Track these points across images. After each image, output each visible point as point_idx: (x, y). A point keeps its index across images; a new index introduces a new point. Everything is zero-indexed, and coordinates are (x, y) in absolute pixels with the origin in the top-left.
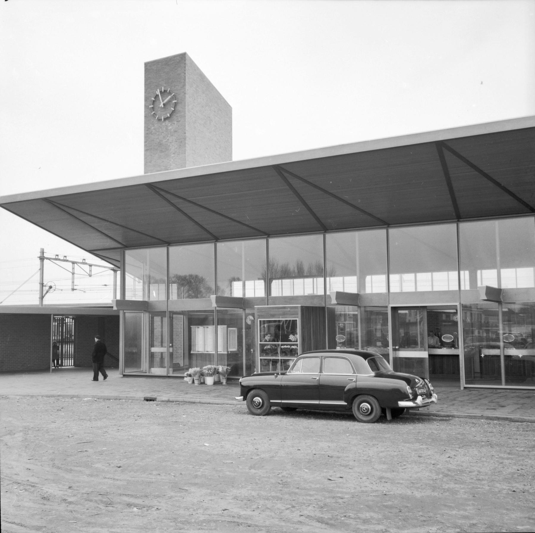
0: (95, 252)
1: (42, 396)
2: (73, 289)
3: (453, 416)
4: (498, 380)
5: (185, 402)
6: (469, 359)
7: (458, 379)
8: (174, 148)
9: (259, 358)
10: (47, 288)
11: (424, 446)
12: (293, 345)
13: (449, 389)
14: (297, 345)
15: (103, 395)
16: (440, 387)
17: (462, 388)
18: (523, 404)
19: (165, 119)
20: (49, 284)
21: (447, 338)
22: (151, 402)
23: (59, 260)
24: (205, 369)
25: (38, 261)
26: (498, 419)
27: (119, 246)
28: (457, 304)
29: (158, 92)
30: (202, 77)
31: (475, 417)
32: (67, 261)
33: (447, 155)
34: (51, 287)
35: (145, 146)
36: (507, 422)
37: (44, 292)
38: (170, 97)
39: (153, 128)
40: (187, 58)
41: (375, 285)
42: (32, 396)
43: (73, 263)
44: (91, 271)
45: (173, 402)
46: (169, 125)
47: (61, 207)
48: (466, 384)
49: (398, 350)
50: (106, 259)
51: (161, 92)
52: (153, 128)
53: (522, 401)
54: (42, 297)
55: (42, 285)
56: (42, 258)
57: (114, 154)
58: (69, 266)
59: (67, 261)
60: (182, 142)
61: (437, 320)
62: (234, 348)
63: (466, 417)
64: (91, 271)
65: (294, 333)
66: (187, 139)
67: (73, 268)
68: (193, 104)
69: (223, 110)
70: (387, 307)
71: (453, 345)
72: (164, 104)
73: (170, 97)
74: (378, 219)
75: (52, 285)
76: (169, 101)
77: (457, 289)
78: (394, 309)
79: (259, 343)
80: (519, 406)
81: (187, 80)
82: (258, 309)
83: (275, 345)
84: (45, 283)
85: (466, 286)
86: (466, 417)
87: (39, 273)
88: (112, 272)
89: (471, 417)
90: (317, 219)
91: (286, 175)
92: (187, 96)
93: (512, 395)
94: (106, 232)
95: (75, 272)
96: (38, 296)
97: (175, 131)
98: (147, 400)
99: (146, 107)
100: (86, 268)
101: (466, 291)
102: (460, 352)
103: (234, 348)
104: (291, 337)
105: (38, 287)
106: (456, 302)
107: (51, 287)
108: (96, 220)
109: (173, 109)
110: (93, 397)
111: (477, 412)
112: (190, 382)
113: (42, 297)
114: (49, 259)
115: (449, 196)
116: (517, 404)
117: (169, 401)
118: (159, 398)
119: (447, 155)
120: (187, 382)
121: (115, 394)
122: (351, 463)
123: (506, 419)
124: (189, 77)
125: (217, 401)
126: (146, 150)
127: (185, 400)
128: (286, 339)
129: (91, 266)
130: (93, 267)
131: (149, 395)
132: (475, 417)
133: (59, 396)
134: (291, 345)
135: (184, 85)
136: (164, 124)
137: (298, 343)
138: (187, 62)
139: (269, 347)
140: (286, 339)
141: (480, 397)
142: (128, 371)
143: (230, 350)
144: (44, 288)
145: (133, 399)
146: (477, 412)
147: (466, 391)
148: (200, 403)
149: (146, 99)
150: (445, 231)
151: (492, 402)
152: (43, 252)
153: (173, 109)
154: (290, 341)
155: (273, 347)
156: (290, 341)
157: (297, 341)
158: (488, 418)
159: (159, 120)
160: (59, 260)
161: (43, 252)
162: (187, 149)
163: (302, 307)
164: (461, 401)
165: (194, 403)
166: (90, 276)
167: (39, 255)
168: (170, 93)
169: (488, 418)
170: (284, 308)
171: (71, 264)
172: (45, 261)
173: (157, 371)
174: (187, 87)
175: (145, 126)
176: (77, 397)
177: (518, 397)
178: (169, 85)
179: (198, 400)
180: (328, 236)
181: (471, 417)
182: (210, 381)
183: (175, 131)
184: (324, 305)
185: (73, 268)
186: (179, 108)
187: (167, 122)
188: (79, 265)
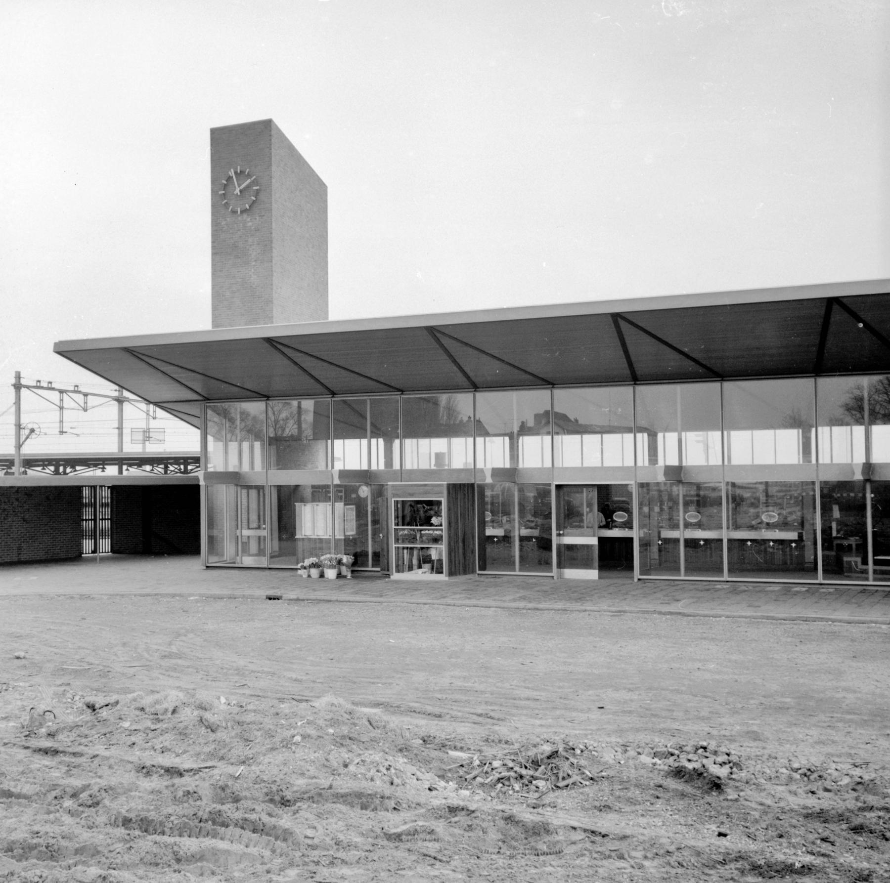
0: (164, 405)
1: (135, 595)
2: (62, 432)
3: (625, 612)
4: (677, 570)
5: (320, 601)
6: (645, 545)
7: (631, 568)
8: (255, 253)
9: (394, 546)
10: (27, 432)
11: (598, 639)
12: (437, 530)
13: (620, 581)
14: (442, 530)
15: (210, 592)
16: (610, 578)
17: (636, 580)
18: (699, 598)
19: (242, 212)
20: (30, 426)
21: (619, 517)
22: (276, 601)
23: (42, 388)
24: (325, 559)
25: (12, 390)
26: (671, 613)
27: (200, 398)
28: (632, 482)
29: (232, 173)
30: (291, 149)
31: (647, 612)
32: (53, 389)
33: (622, 324)
34: (32, 431)
35: (213, 247)
36: (680, 617)
37: (23, 438)
38: (249, 181)
39: (224, 223)
40: (273, 127)
41: (537, 454)
42: (122, 596)
43: (61, 392)
44: (86, 403)
45: (303, 600)
46: (249, 220)
47: (143, 357)
48: (641, 574)
49: (563, 535)
50: (175, 413)
51: (236, 173)
52: (224, 223)
53: (699, 594)
54: (19, 446)
55: (19, 427)
56: (18, 387)
57: (181, 302)
58: (54, 396)
59: (53, 389)
60: (267, 245)
61: (609, 501)
62: (352, 530)
63: (638, 612)
64: (86, 403)
65: (438, 514)
66: (274, 241)
67: (62, 400)
68: (281, 192)
69: (316, 191)
70: (550, 485)
71: (628, 525)
72: (241, 191)
73: (249, 181)
74: (543, 379)
75: (35, 426)
76: (248, 187)
77: (632, 464)
78: (558, 487)
79: (394, 527)
80: (695, 600)
81: (273, 159)
82: (393, 486)
83: (414, 530)
84: (24, 420)
85: (643, 460)
86: (638, 612)
87: (13, 409)
88: (116, 403)
89: (644, 612)
90: (468, 377)
91: (438, 335)
92: (274, 181)
93: (692, 587)
94: (186, 383)
95: (65, 406)
96: (12, 441)
97: (257, 230)
98: (270, 599)
99: (214, 192)
100: (80, 398)
101: (644, 467)
102: (635, 534)
103: (352, 532)
104: (434, 520)
105: (12, 430)
106: (631, 480)
107: (32, 431)
108: (163, 364)
109: (254, 198)
110: (201, 595)
111: (650, 607)
112: (305, 576)
113: (19, 446)
114: (28, 387)
115: (625, 360)
116: (693, 597)
117: (298, 600)
118: (285, 596)
119: (622, 324)
120: (301, 576)
121: (226, 592)
122: (536, 653)
123: (679, 614)
124: (277, 153)
125: (358, 598)
126: (214, 254)
127: (319, 598)
128: (427, 522)
129: (86, 395)
130: (89, 397)
131: (271, 593)
132: (647, 612)
133: (156, 595)
134: (433, 530)
135: (271, 165)
136: (240, 218)
137: (443, 527)
138: (273, 132)
139: (406, 532)
140: (427, 522)
141: (655, 590)
142: (213, 560)
143: (348, 533)
144: (22, 432)
145: (252, 597)
146: (650, 607)
147: (640, 582)
148: (337, 601)
149: (214, 181)
150: (620, 395)
151: (667, 595)
152: (18, 376)
153: (254, 198)
154: (432, 525)
155: (412, 532)
156: (432, 525)
157: (441, 525)
158: (660, 613)
159: (234, 212)
160: (42, 388)
161: (18, 376)
162: (274, 255)
163: (449, 485)
164: (634, 595)
165: (330, 601)
166: (85, 410)
167: (13, 381)
168: (249, 176)
169: (660, 613)
170: (426, 485)
171: (57, 393)
172: (23, 390)
173: (248, 561)
174: (274, 168)
175: (212, 220)
176: (180, 595)
177: (697, 590)
178: (250, 169)
179: (334, 598)
180: (478, 395)
181: (644, 612)
182: (331, 574)
183: (257, 230)
184: (473, 481)
185: (62, 400)
186: (262, 196)
187: (245, 216)
188: (70, 394)
